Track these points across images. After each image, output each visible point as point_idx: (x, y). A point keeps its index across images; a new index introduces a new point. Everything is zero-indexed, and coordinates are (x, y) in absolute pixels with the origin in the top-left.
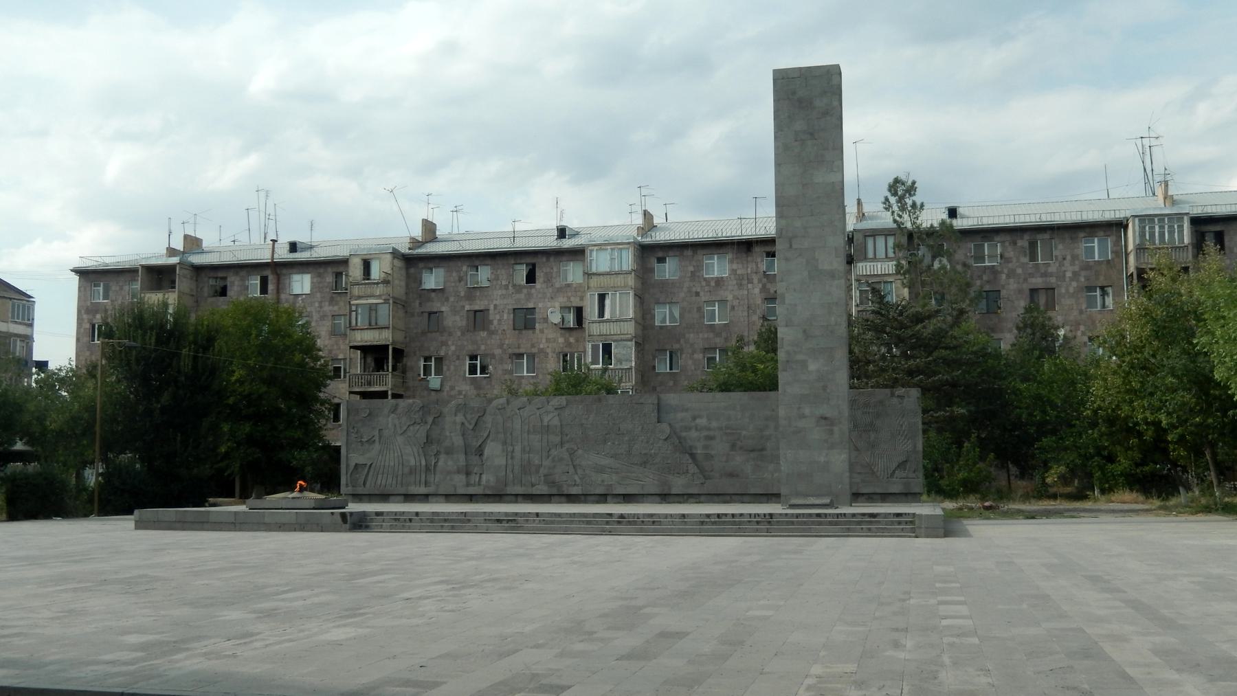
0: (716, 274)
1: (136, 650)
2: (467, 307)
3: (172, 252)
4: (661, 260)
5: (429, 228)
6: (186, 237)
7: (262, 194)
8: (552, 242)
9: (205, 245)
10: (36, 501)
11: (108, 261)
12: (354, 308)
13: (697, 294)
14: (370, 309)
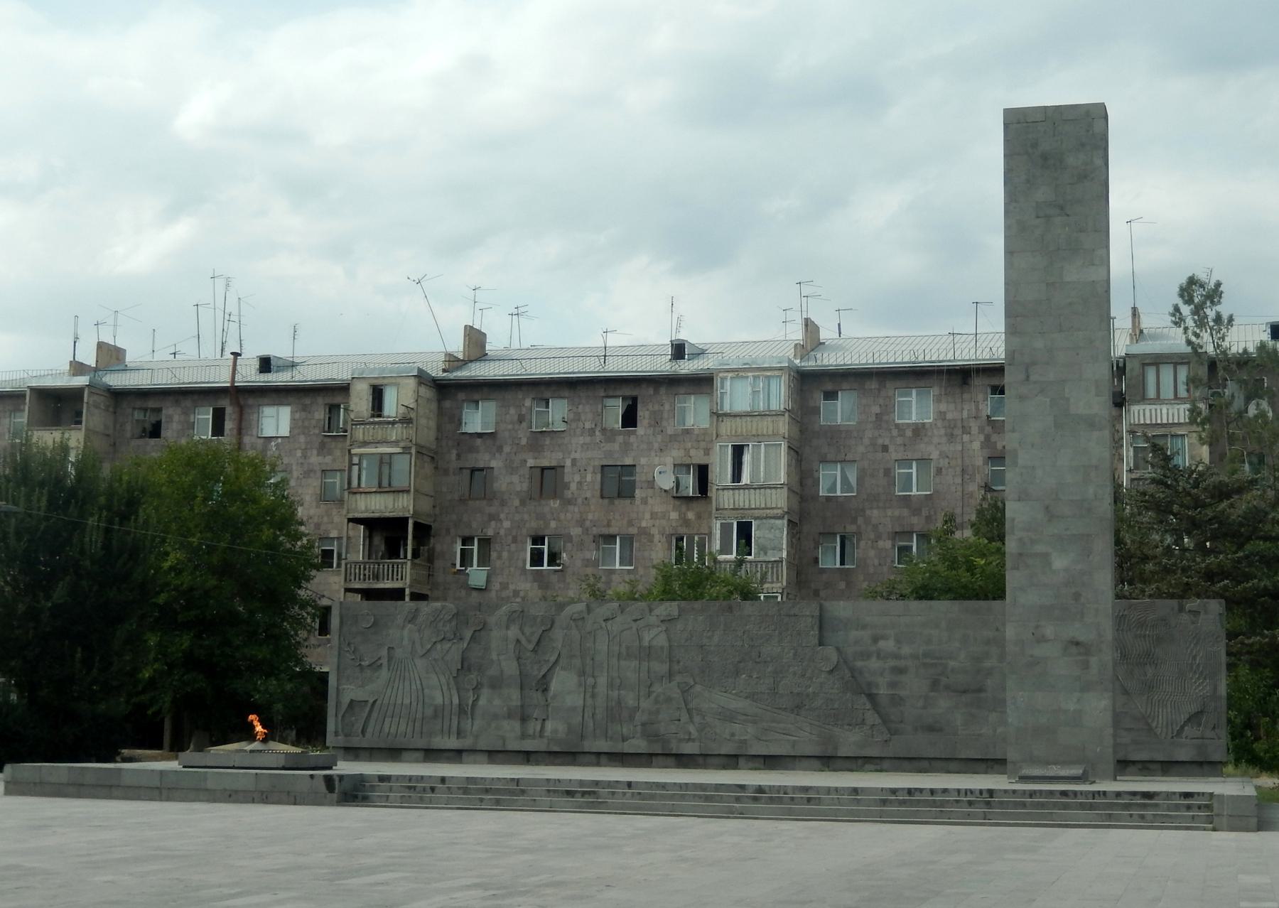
0: (914, 419)
2: (531, 462)
4: (831, 395)
6: (101, 346)
7: (220, 284)
8: (663, 365)
12: (356, 460)
13: (885, 449)
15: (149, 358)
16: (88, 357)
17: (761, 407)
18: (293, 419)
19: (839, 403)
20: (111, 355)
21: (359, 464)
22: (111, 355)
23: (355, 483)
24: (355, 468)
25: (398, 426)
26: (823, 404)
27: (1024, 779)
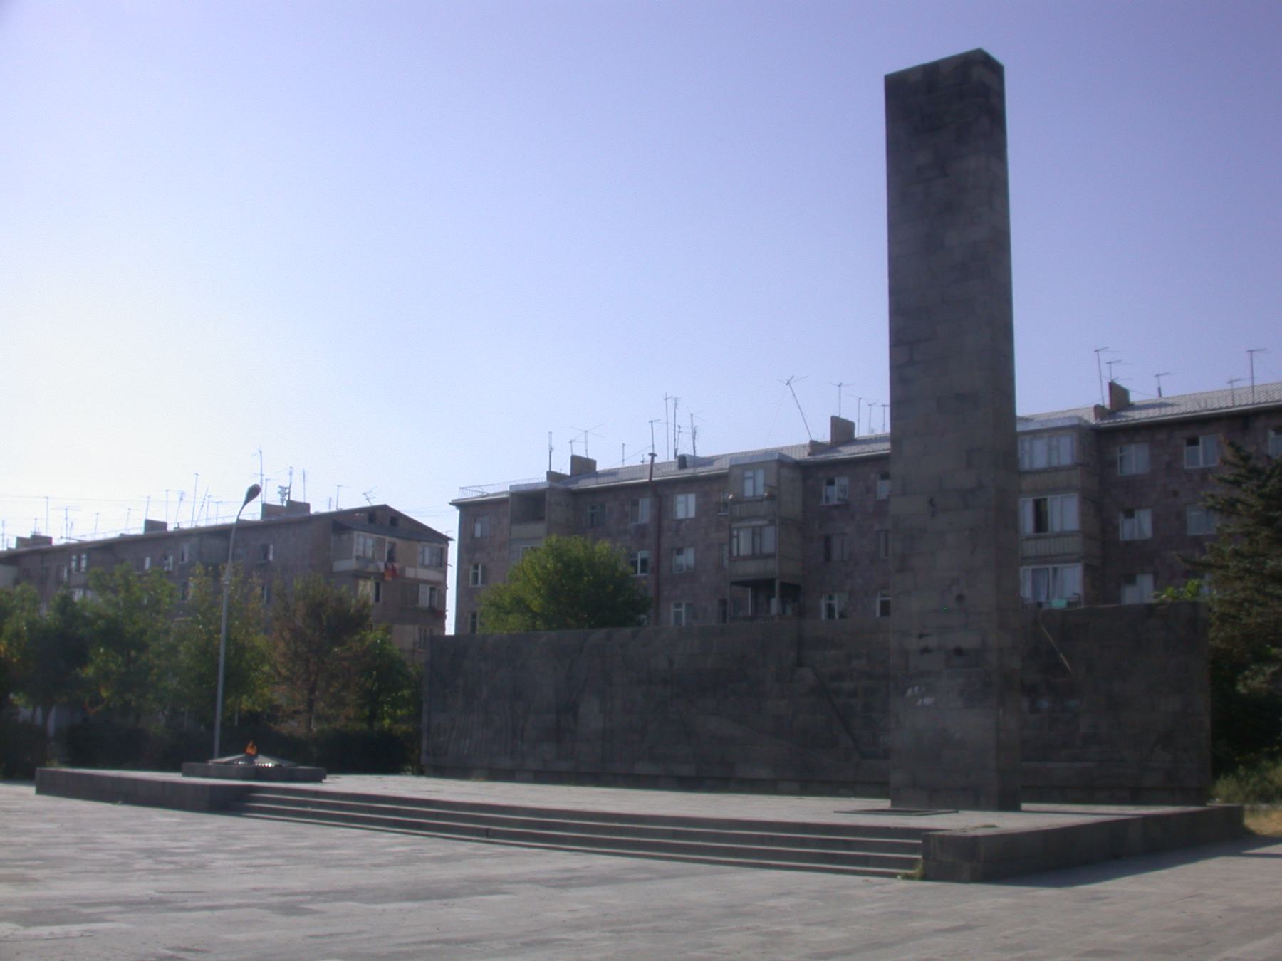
0: (1201, 464)
1: (168, 949)
2: (877, 527)
3: (552, 476)
4: (1193, 442)
5: (1118, 394)
6: (575, 460)
7: (671, 403)
8: (675, 473)
9: (599, 468)
10: (15, 772)
11: (491, 491)
12: (735, 533)
13: (1175, 494)
14: (754, 534)
15: (620, 466)
16: (824, 435)
17: (1055, 463)
18: (697, 504)
19: (1200, 448)
20: (582, 466)
21: (738, 537)
22: (582, 466)
23: (735, 553)
24: (735, 540)
25: (766, 503)
26: (1187, 450)
27: (157, 862)
